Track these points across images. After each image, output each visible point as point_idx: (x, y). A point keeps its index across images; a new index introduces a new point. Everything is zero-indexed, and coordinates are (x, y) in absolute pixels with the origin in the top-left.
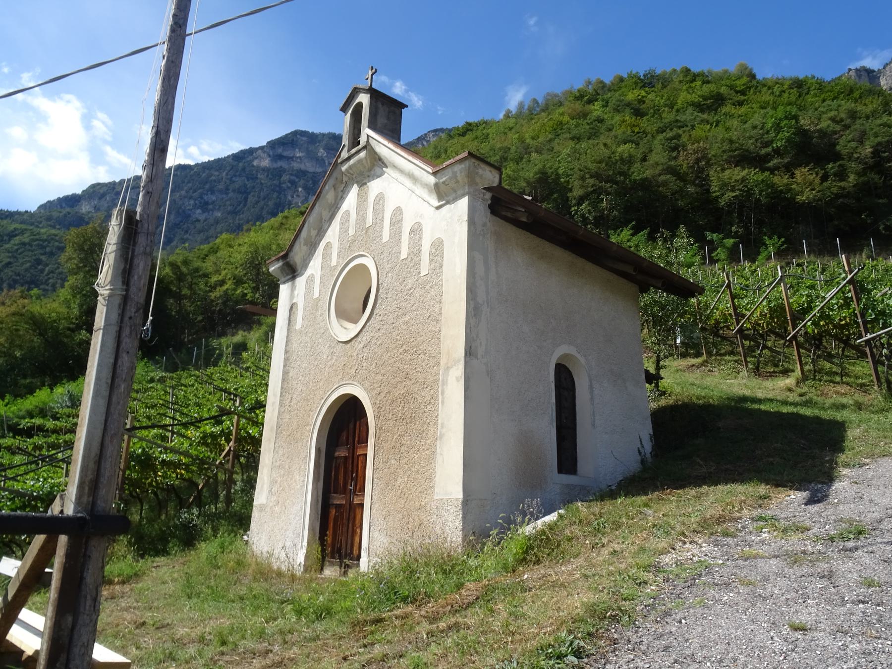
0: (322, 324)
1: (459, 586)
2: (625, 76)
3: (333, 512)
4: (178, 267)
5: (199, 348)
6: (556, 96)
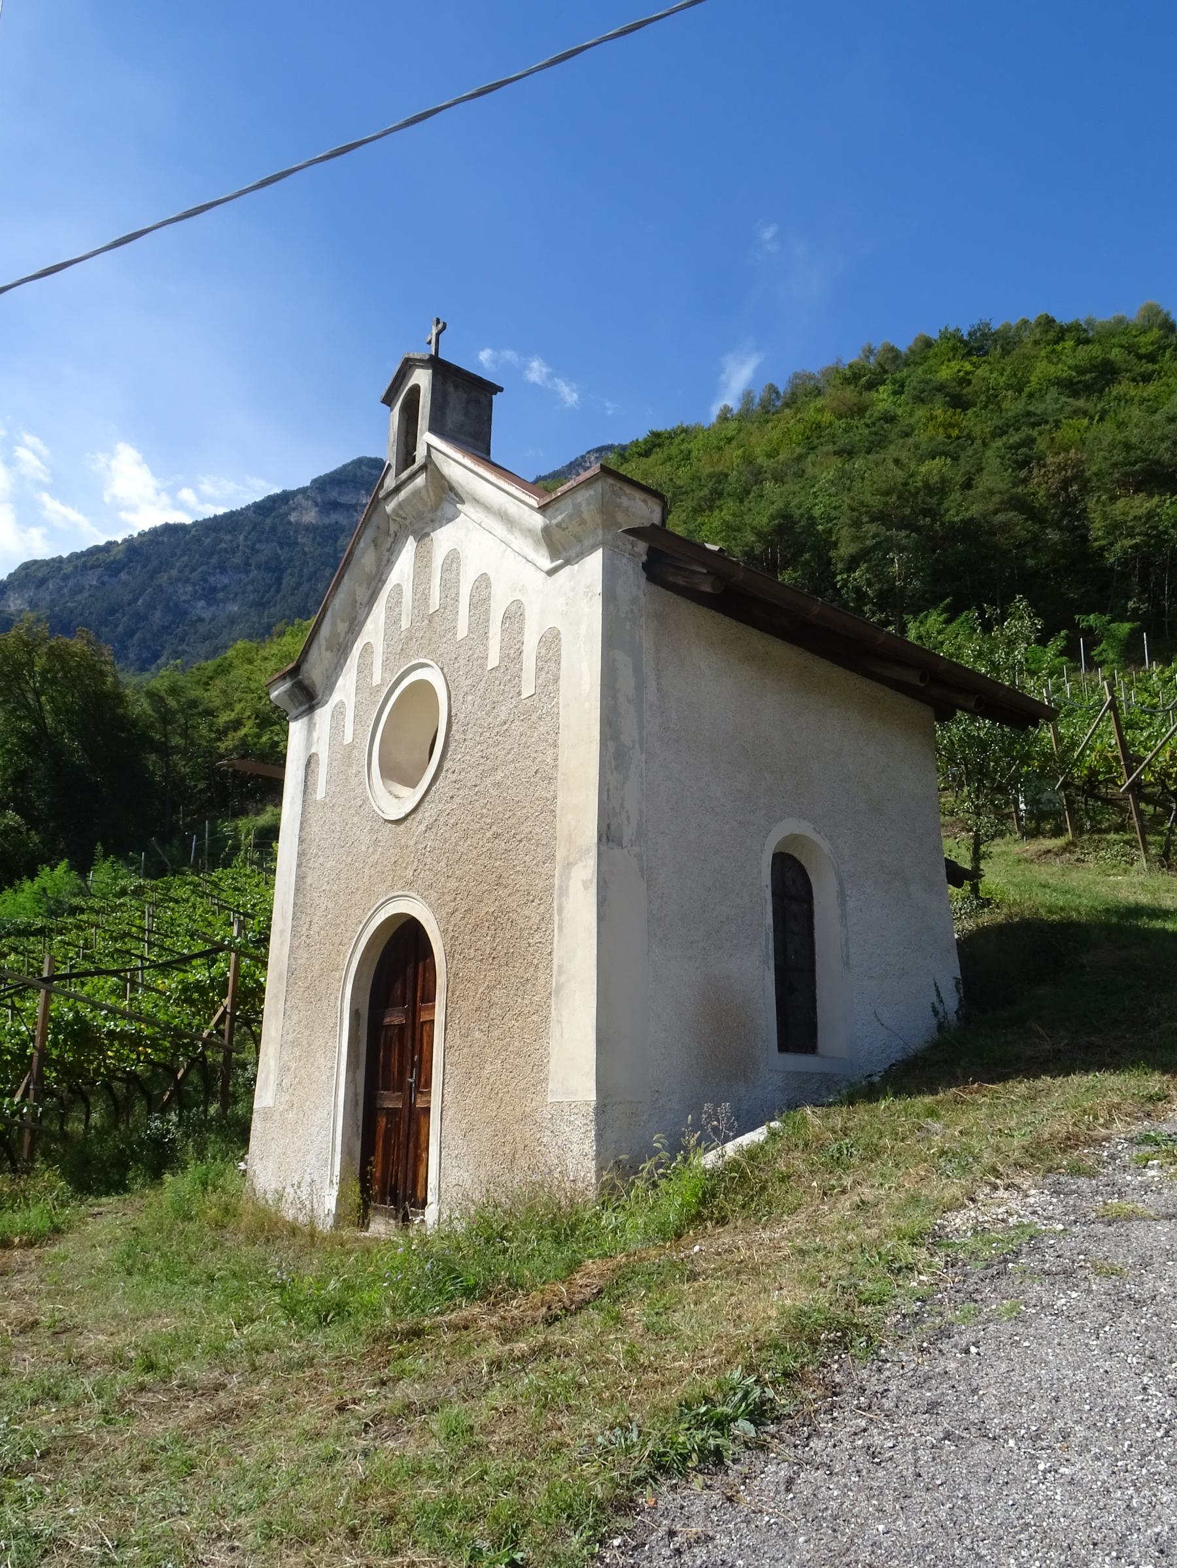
0: (359, 790)
1: (574, 1266)
2: (935, 336)
3: (382, 1122)
4: (162, 699)
5: (201, 837)
6: (811, 377)
